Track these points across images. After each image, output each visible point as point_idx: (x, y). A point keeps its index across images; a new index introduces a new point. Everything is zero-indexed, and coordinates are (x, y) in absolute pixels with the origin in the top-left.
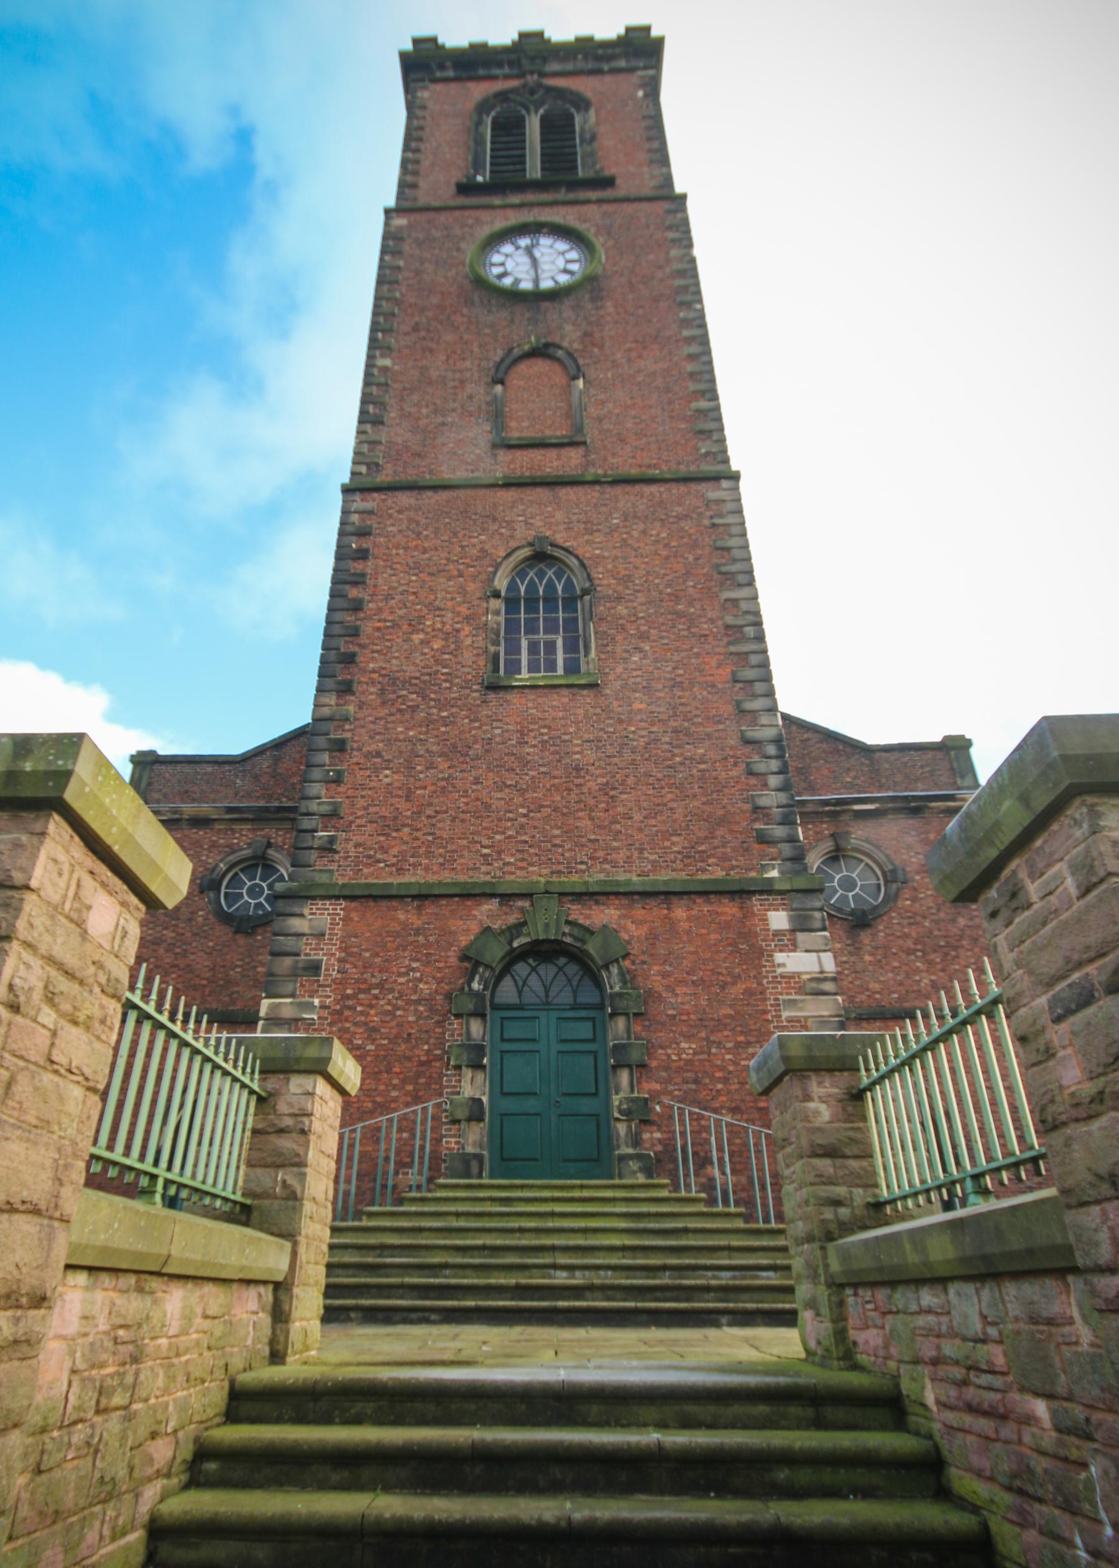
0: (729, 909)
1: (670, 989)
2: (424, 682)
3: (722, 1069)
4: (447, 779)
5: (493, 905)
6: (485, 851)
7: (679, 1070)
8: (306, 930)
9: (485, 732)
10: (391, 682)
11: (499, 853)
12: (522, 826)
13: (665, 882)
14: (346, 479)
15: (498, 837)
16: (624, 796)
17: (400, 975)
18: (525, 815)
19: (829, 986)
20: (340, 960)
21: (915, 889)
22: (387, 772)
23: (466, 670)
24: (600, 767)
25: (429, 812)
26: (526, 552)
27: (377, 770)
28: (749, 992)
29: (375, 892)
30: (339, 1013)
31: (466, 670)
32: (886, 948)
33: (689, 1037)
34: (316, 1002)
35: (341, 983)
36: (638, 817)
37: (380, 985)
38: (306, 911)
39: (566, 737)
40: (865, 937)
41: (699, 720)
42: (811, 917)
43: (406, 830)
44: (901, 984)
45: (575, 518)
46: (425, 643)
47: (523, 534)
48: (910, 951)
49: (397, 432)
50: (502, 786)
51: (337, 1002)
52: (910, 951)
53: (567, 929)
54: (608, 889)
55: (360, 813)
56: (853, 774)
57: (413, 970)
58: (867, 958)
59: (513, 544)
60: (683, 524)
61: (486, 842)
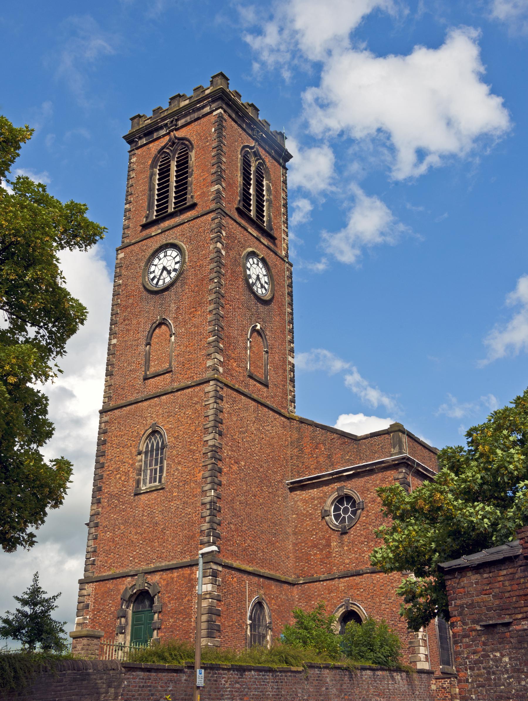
0: (187, 571)
1: (169, 602)
2: (119, 495)
3: (178, 627)
4: (122, 533)
5: (129, 579)
6: (131, 559)
7: (169, 628)
8: (86, 594)
9: (134, 513)
10: (111, 496)
11: (134, 558)
12: (141, 548)
13: (165, 566)
14: (101, 408)
15: (135, 553)
16: (167, 532)
17: (107, 605)
18: (142, 544)
19: (208, 596)
20: (94, 603)
21: (368, 511)
22: (108, 533)
23: (130, 488)
24: (162, 522)
25: (118, 547)
26: (150, 431)
27: (106, 532)
28: (188, 600)
29: (102, 579)
30: (93, 620)
31: (130, 488)
32: (353, 542)
33: (172, 617)
34: (88, 617)
35: (93, 610)
36: (170, 539)
37: (102, 610)
38: (86, 588)
39: (154, 511)
40: (346, 537)
41: (191, 497)
42: (207, 572)
43: (112, 554)
44: (357, 559)
45: (165, 410)
46: (120, 478)
47: (150, 421)
48: (362, 543)
49: (117, 379)
50: (137, 533)
51: (93, 616)
52: (362, 543)
53: (146, 585)
54: (157, 569)
55: (101, 550)
56: (349, 455)
57: (110, 603)
58: (346, 548)
59: (146, 428)
60: (196, 406)
61: (131, 555)
